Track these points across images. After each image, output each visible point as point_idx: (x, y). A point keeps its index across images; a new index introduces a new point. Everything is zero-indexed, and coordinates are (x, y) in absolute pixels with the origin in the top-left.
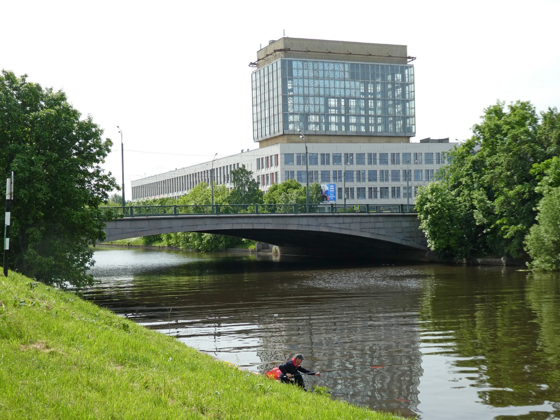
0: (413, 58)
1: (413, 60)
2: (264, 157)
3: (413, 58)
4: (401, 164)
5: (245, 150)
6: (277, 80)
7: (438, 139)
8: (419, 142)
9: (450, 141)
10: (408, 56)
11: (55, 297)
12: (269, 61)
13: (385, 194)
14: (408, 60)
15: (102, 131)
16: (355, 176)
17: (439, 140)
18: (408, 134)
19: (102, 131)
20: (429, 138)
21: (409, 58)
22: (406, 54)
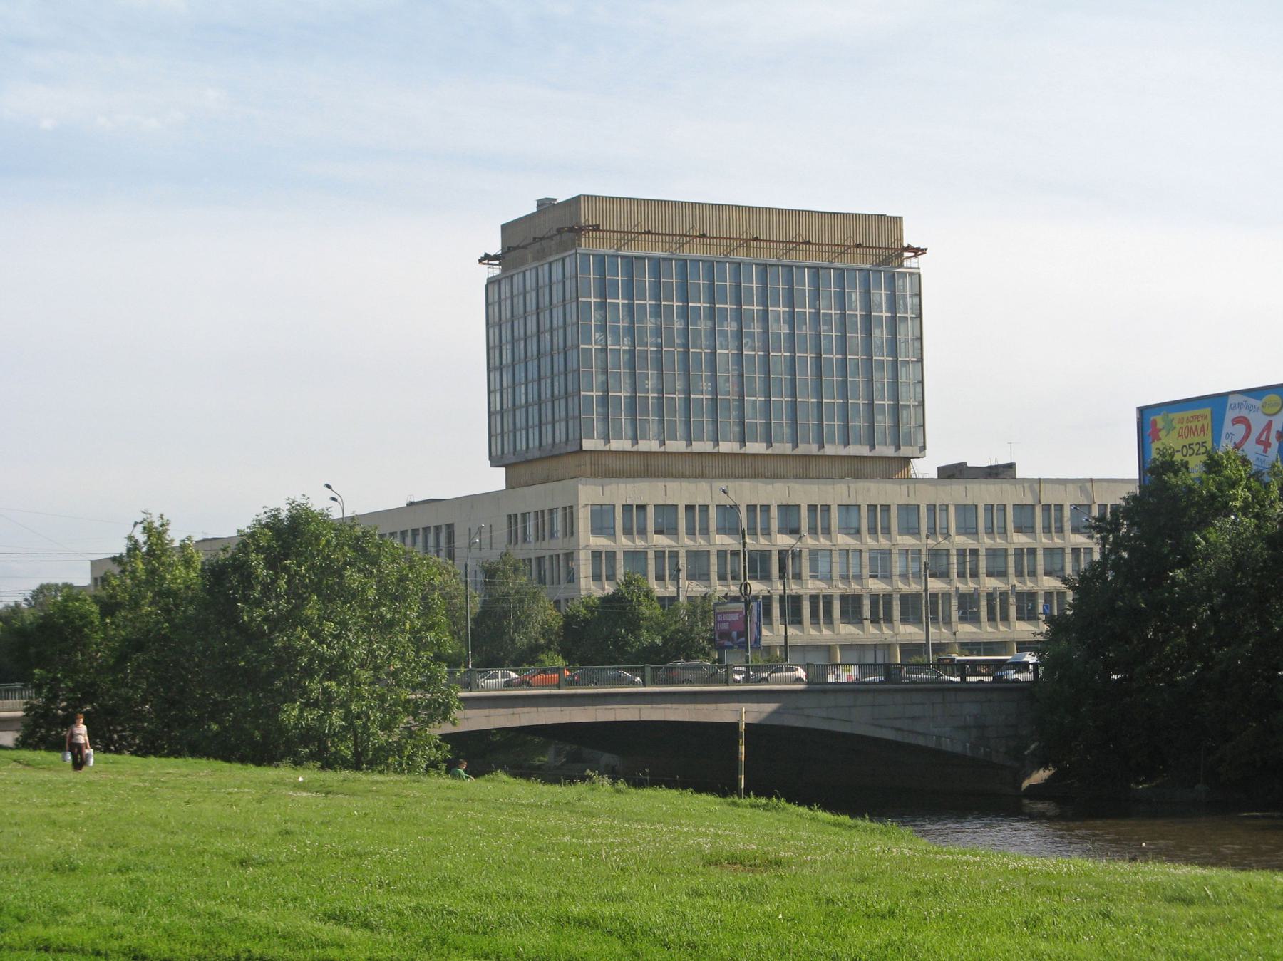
0: (918, 249)
1: (916, 256)
2: (561, 552)
3: (919, 252)
4: (1041, 593)
5: (330, 494)
6: (564, 306)
7: (985, 464)
8: (935, 476)
9: (1020, 474)
10: (906, 245)
11: (1087, 861)
12: (541, 255)
13: (695, 607)
14: (906, 254)
15: (239, 531)
16: (714, 568)
17: (990, 468)
18: (905, 451)
19: (239, 531)
20: (964, 464)
21: (909, 249)
22: (900, 238)
